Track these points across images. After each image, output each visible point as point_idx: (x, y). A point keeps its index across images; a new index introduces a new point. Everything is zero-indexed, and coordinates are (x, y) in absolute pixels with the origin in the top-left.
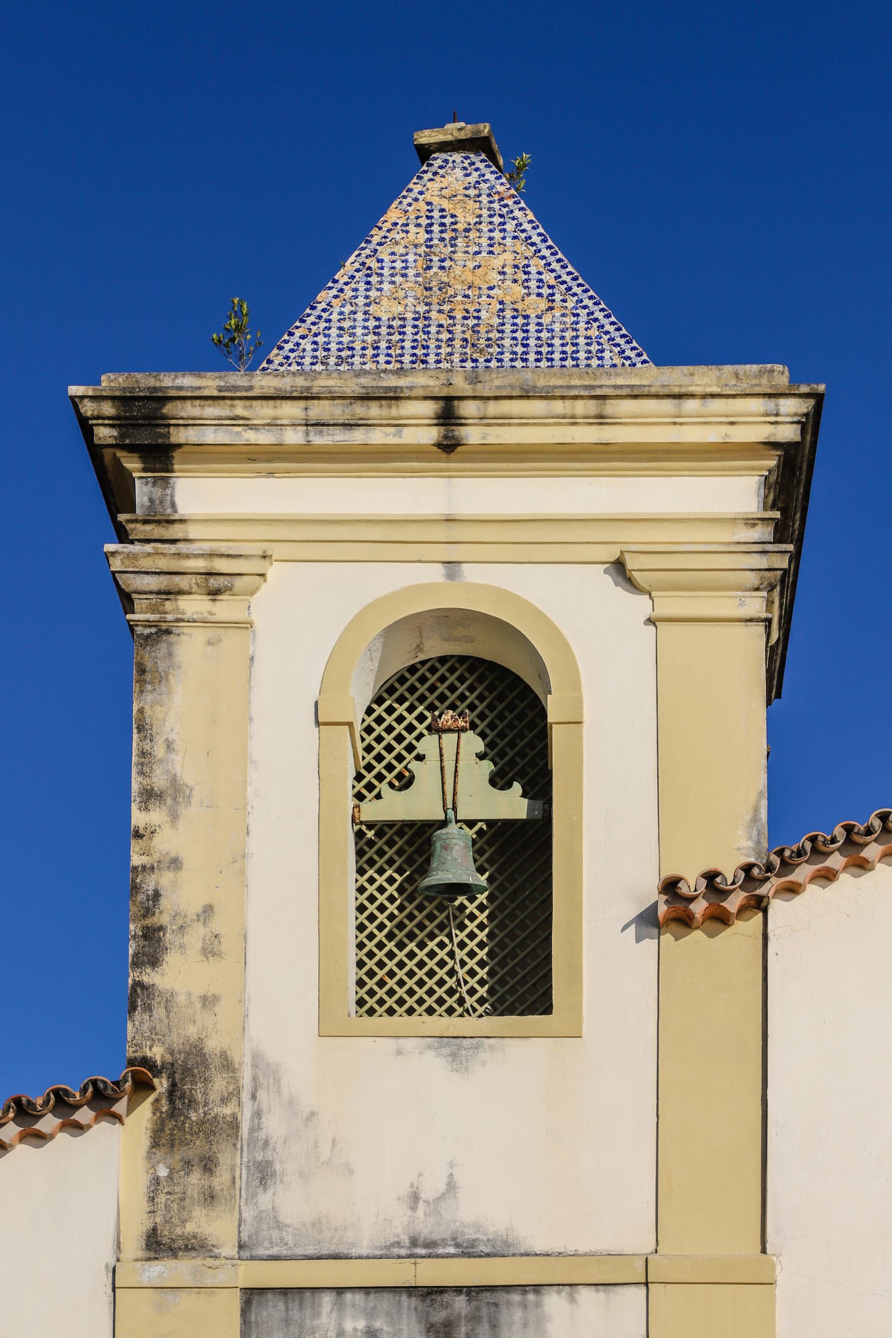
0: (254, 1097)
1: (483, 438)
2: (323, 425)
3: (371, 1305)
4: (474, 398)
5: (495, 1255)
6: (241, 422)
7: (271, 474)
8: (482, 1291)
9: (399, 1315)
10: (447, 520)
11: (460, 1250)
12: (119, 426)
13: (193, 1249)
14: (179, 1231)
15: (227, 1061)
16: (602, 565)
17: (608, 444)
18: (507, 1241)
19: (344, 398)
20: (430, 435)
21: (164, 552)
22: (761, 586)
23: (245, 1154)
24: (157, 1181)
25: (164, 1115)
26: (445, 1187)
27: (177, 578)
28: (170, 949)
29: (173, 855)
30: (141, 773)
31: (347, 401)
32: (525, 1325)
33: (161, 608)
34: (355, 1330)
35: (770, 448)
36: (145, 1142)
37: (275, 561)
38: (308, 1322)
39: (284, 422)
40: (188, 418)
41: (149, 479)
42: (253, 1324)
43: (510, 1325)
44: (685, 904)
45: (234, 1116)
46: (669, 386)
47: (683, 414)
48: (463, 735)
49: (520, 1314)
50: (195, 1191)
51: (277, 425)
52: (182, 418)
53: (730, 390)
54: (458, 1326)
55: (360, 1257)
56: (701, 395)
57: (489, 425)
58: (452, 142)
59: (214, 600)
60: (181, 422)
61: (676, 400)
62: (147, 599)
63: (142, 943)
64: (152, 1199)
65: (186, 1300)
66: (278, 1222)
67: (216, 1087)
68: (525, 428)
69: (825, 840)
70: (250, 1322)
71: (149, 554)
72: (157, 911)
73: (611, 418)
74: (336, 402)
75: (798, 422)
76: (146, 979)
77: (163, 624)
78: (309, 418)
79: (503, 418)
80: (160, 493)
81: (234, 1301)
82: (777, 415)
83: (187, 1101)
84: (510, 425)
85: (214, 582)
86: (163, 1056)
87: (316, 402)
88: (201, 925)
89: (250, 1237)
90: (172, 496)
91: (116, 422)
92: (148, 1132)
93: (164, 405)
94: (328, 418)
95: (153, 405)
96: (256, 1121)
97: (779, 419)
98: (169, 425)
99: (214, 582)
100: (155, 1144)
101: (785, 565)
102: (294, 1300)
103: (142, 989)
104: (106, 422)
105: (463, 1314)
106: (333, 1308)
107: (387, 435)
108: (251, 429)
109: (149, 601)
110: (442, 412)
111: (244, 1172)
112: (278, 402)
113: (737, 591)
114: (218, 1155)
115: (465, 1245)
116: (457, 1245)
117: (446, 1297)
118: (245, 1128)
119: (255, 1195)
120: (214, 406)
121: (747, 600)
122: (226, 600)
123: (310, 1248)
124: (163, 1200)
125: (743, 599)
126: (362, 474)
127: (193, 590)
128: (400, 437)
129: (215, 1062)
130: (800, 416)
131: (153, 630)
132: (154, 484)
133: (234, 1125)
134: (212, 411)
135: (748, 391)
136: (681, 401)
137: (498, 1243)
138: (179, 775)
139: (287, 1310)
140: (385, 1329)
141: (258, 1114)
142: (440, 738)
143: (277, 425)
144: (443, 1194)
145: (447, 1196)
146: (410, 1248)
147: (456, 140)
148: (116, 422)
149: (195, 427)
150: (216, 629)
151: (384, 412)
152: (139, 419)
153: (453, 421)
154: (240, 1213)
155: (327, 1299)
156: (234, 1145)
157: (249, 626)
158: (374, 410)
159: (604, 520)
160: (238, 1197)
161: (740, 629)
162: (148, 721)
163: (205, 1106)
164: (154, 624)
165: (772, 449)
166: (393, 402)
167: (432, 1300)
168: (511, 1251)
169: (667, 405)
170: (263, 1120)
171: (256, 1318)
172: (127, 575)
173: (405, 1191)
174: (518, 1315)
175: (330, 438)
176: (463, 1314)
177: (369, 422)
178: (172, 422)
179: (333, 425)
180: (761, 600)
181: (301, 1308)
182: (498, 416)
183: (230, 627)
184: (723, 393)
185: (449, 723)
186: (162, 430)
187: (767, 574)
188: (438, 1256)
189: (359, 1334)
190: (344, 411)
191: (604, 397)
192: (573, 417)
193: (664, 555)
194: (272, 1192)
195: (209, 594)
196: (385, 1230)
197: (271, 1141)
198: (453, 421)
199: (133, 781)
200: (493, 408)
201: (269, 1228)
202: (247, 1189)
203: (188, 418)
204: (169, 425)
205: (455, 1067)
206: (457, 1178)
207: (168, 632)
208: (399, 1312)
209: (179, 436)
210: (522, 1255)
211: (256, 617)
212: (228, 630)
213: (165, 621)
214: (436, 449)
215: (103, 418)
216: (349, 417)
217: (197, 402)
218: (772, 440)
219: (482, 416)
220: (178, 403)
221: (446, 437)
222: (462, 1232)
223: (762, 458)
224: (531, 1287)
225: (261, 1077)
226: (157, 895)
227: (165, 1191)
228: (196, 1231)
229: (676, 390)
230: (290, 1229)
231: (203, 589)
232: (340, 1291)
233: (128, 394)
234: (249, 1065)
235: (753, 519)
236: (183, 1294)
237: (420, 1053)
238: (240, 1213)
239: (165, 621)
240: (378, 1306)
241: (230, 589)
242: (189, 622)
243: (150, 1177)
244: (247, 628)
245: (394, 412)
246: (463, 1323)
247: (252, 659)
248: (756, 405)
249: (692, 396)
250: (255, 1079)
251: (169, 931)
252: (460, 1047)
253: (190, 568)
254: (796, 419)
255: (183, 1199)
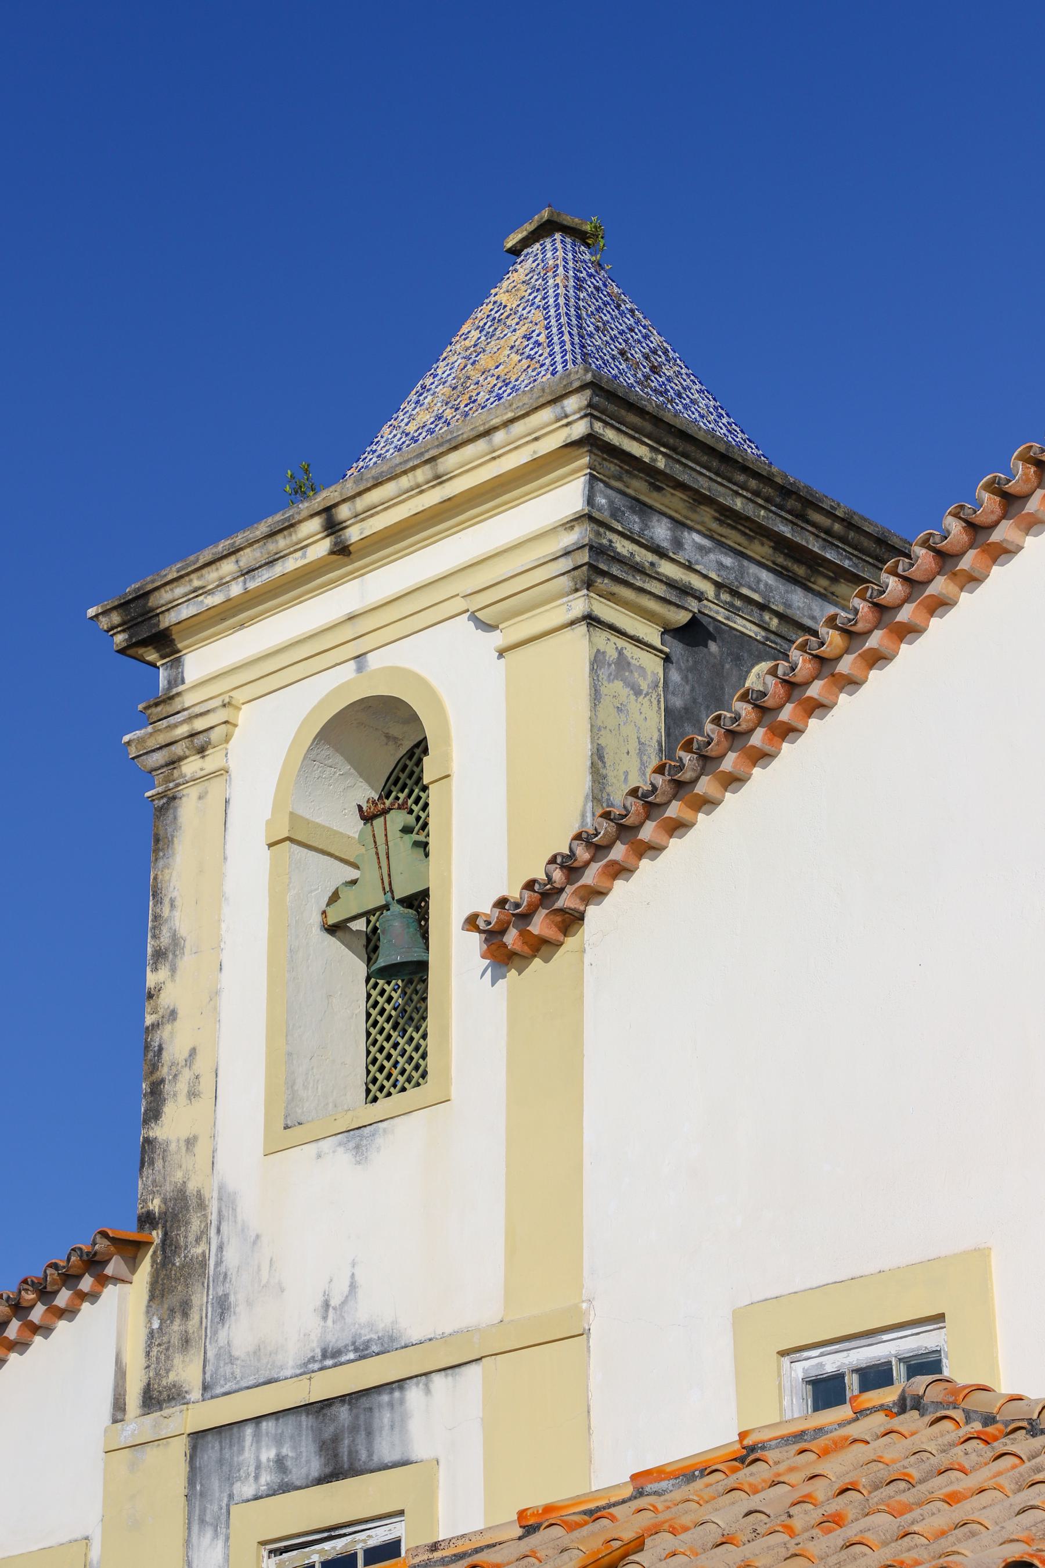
0: (219, 1231)
1: (361, 533)
2: (253, 570)
3: (280, 1431)
4: (344, 501)
5: (383, 1353)
6: (201, 592)
7: (242, 626)
8: (360, 1396)
9: (300, 1437)
10: (349, 619)
11: (358, 1354)
12: (128, 628)
13: (174, 1398)
14: (164, 1383)
15: (201, 1199)
16: (464, 615)
17: (449, 499)
18: (392, 1337)
19: (257, 541)
20: (322, 548)
21: (160, 728)
22: (578, 586)
23: (211, 1292)
24: (151, 1334)
25: (159, 1266)
26: (348, 1289)
27: (173, 748)
28: (167, 1099)
29: (171, 1008)
30: (155, 937)
31: (261, 543)
32: (392, 1427)
33: (171, 778)
34: (268, 1460)
35: (576, 448)
36: (145, 1297)
37: (243, 704)
38: (235, 1459)
39: (228, 579)
40: (167, 604)
41: (168, 664)
42: (198, 1470)
43: (381, 1429)
44: (499, 937)
45: (203, 1253)
46: (476, 427)
47: (496, 448)
48: (388, 816)
49: (388, 1415)
50: (176, 1339)
51: (224, 584)
52: (163, 605)
53: (521, 410)
54: (342, 1440)
55: (286, 1379)
56: (502, 425)
57: (363, 520)
58: (527, 236)
59: (203, 757)
60: (164, 608)
61: (487, 438)
62: (161, 773)
63: (150, 1099)
64: (148, 1354)
65: (151, 1452)
66: (231, 1356)
67: (194, 1228)
68: (389, 511)
69: (588, 835)
70: (196, 1468)
71: (151, 734)
72: (160, 1064)
73: (446, 475)
74: (255, 546)
75: (585, 416)
76: (151, 1134)
77: (169, 792)
78: (242, 568)
79: (371, 510)
80: (175, 673)
81: (180, 1447)
82: (566, 416)
83: (173, 1248)
84: (377, 513)
85: (198, 741)
86: (160, 1207)
87: (242, 553)
88: (187, 1069)
89: (212, 1376)
90: (182, 672)
91: (125, 627)
92: (148, 1286)
93: (149, 599)
94: (254, 562)
95: (141, 602)
96: (219, 1255)
97: (570, 419)
98: (158, 615)
99: (198, 741)
100: (152, 1298)
101: (586, 559)
102: (226, 1438)
103: (148, 1145)
104: (119, 629)
105: (346, 1425)
106: (253, 1440)
107: (296, 559)
108: (209, 594)
109: (163, 775)
110: (327, 524)
111: (210, 1309)
112: (218, 564)
113: (562, 598)
114: (192, 1298)
115: (361, 1348)
116: (356, 1350)
117: (334, 1409)
118: (212, 1263)
119: (215, 1333)
120: (179, 586)
121: (572, 604)
122: (211, 754)
123: (251, 1378)
124: (155, 1353)
125: (569, 604)
126: (301, 599)
127: (187, 754)
128: (305, 558)
129: (193, 1202)
130: (584, 409)
131: (165, 800)
132: (171, 667)
133: (203, 1263)
134: (179, 590)
135: (535, 405)
136: (491, 436)
137: (386, 1339)
138: (177, 930)
139: (221, 1450)
140: (290, 1454)
141: (221, 1248)
142: (372, 824)
143: (224, 584)
144: (347, 1297)
145: (349, 1298)
146: (321, 1361)
147: (529, 234)
148: (125, 627)
149: (174, 609)
150: (203, 783)
151: (288, 541)
152: (137, 618)
153: (338, 527)
154: (205, 1353)
155: (249, 1431)
156: (203, 1283)
157: (222, 772)
158: (281, 542)
159: (465, 568)
160: (204, 1337)
161: (568, 634)
162: (159, 886)
163: (185, 1249)
164: (163, 794)
165: (580, 448)
166: (292, 529)
167: (324, 1415)
168: (396, 1345)
169: (481, 445)
170: (224, 1253)
171: (200, 1463)
172: (142, 758)
173: (319, 1302)
174: (386, 1416)
175: (260, 580)
176: (346, 1425)
177: (282, 554)
178: (158, 611)
179: (260, 567)
180: (583, 598)
181: (231, 1446)
182: (366, 509)
183: (212, 778)
184: (517, 415)
185: (372, 810)
186: (154, 621)
187: (576, 573)
188: (341, 1364)
189: (271, 1463)
190: (261, 553)
191: (433, 459)
192: (419, 486)
193: (494, 588)
194: (228, 1326)
195: (199, 753)
196: (305, 1345)
197: (229, 1273)
198: (338, 527)
199: (149, 945)
200: (361, 503)
201: (225, 1364)
202: (211, 1327)
203: (167, 604)
204: (158, 615)
205: (358, 1159)
206: (360, 1279)
207: (174, 798)
208: (300, 1435)
209: (168, 620)
210: (402, 1348)
211: (232, 765)
212: (211, 781)
213: (170, 790)
214: (334, 557)
215: (116, 627)
216: (267, 556)
217: (168, 588)
218: (569, 441)
219: (354, 514)
220: (156, 594)
221: (336, 544)
222: (360, 1334)
223: (577, 459)
224: (397, 1384)
225: (224, 1209)
226: (161, 1049)
227: (157, 1343)
228: (175, 1379)
229: (482, 429)
230: (239, 1362)
231: (192, 750)
232: (258, 1420)
233: (122, 601)
234: (216, 1199)
235: (568, 522)
236: (148, 1448)
237: (334, 1152)
238: (205, 1353)
239: (170, 790)
240: (285, 1430)
241: (208, 743)
242: (184, 784)
243: (148, 1330)
244: (222, 774)
245: (294, 538)
246: (346, 1435)
247: (227, 802)
248: (546, 415)
249: (495, 429)
250: (220, 1212)
251: (167, 1081)
252: (362, 1137)
253: (178, 735)
254: (582, 413)
255: (167, 1349)
